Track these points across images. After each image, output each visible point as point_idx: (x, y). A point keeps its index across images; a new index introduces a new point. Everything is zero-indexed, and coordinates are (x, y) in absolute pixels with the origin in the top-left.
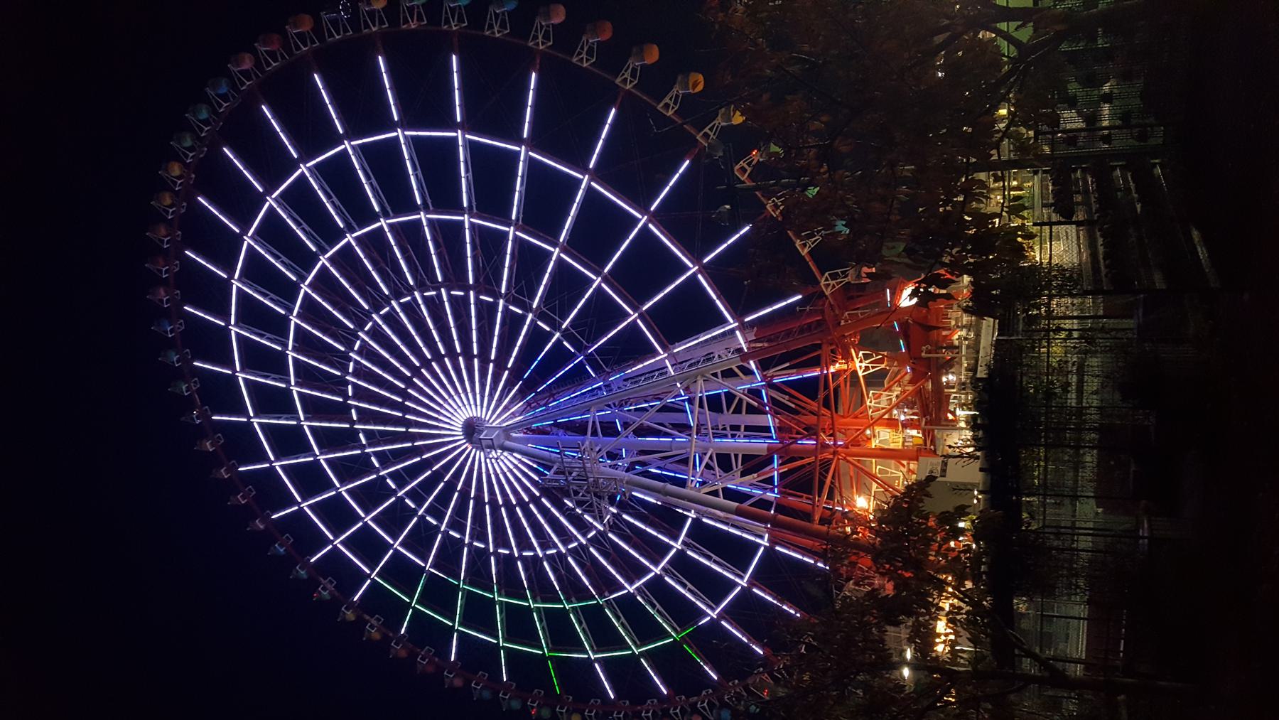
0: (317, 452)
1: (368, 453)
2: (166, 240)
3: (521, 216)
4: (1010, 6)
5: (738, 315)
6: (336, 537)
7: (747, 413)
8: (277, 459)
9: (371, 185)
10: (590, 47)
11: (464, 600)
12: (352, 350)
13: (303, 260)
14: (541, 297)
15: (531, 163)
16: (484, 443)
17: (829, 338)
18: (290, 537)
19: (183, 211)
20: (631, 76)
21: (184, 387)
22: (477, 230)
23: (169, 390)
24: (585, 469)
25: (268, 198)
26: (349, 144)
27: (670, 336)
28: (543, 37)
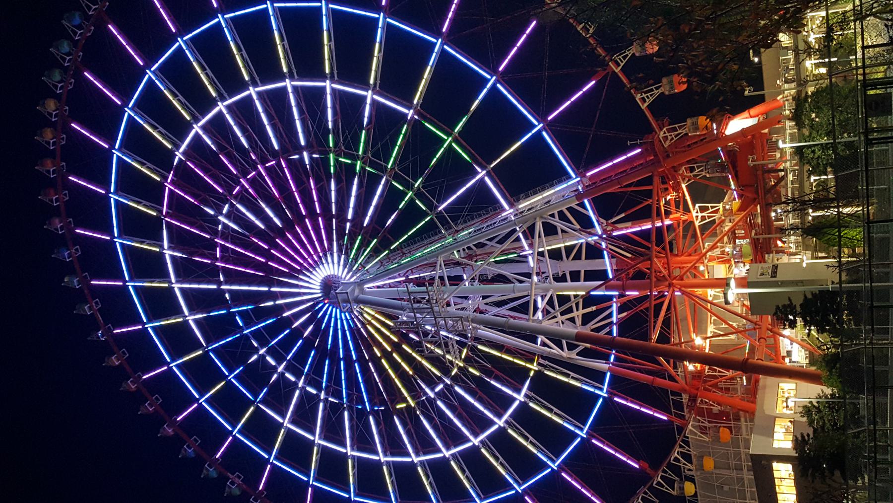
0: (173, 280)
1: (223, 290)
3: (378, 82)
4: (775, 434)
8: (131, 280)
9: (242, 56)
12: (221, 214)
13: (178, 129)
14: (396, 158)
15: (389, 28)
16: (340, 297)
18: (159, 398)
21: (66, 254)
22: (337, 94)
23: (53, 256)
24: (432, 309)
25: (147, 71)
26: (223, 17)
27: (515, 193)
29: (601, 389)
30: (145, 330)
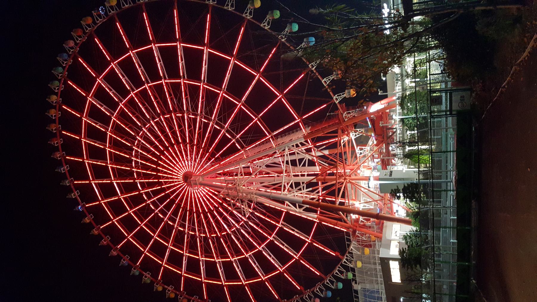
2: (60, 75)
5: (300, 115)
6: (114, 218)
7: (308, 166)
10: (250, 11)
17: (341, 127)
19: (70, 64)
20: (267, 24)
28: (231, 6)
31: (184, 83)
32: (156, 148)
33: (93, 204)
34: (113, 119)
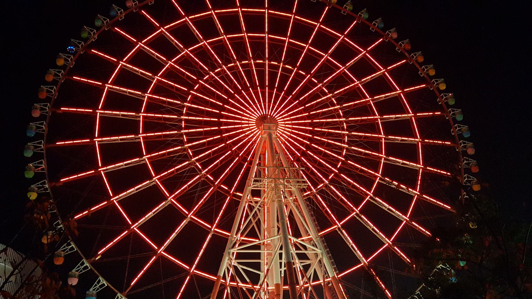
11: (242, 26)
29: (98, 141)
30: (365, 49)
31: (336, 224)
32: (322, 134)
33: (315, 32)
34: (382, 135)
